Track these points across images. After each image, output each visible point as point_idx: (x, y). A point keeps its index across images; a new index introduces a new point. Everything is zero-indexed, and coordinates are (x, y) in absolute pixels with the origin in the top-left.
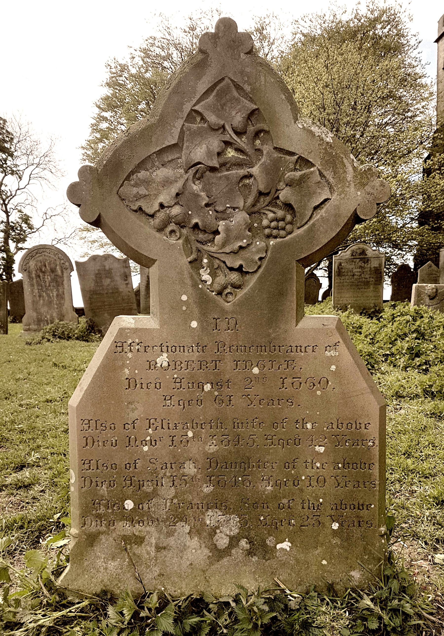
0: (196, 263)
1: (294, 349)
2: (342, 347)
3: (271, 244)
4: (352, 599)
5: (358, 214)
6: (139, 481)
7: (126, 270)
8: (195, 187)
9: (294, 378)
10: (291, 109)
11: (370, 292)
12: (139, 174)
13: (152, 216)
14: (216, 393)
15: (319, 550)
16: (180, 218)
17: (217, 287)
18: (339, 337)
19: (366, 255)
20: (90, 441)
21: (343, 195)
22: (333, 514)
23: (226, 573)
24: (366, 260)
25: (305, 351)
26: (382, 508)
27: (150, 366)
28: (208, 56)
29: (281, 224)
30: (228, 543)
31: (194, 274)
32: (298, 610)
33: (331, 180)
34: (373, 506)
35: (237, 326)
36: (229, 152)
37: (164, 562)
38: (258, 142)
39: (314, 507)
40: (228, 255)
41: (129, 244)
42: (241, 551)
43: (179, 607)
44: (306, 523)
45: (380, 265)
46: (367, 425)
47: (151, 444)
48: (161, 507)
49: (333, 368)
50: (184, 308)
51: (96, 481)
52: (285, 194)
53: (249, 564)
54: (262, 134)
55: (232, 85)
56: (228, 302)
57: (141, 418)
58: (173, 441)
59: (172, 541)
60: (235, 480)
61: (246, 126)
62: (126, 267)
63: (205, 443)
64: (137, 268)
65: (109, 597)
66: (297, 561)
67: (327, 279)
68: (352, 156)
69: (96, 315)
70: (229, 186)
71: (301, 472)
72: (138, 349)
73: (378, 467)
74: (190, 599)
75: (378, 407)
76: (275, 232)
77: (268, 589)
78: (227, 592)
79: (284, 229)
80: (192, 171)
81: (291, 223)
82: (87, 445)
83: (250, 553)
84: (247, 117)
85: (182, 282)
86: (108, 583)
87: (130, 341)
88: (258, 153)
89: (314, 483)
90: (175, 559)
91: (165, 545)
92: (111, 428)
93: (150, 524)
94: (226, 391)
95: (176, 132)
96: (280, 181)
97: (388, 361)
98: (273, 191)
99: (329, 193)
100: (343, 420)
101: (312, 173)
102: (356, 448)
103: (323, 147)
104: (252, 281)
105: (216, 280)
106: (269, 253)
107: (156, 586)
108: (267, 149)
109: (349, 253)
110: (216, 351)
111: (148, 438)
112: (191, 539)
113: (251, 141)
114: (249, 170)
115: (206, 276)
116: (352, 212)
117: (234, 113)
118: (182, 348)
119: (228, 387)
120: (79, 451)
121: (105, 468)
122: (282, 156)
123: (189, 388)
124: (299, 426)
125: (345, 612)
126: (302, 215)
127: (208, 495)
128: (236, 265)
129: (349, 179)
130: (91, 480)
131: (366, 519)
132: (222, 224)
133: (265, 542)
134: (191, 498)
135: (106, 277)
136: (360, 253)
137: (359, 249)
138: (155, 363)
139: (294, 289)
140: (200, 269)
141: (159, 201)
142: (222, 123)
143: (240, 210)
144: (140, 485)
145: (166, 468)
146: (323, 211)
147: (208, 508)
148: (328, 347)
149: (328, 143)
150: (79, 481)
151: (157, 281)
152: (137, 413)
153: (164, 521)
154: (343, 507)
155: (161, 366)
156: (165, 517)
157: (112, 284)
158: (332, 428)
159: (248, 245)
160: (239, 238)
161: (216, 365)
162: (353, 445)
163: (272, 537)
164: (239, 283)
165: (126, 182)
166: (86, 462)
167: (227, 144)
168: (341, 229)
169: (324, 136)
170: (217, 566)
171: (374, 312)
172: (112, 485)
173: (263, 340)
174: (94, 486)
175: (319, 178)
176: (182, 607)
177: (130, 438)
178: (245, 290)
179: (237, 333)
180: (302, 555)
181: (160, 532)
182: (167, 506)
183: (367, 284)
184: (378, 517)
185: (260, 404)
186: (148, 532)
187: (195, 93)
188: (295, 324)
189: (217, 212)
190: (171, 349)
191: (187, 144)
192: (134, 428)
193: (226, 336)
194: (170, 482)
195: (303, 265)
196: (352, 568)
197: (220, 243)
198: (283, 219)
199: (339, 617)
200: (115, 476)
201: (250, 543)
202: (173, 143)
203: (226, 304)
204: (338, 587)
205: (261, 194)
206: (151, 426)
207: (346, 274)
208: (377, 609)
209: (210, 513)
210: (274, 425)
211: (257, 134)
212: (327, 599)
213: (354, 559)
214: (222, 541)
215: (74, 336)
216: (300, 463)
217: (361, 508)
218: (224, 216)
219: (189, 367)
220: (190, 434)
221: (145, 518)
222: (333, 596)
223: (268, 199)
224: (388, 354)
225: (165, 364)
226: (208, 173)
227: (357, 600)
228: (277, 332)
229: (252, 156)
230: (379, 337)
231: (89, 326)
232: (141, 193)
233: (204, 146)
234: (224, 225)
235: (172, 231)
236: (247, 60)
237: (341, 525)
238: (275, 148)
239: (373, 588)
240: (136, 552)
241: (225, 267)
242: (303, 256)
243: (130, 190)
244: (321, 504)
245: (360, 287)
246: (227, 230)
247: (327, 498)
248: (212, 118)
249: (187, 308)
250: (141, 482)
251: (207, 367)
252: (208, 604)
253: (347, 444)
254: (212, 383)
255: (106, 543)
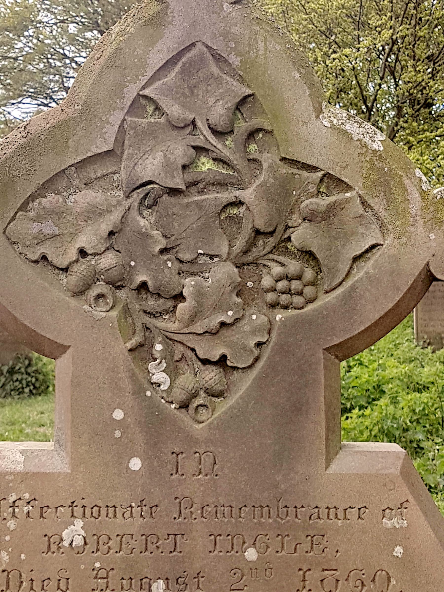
0: (141, 351)
1: (324, 512)
2: (413, 509)
3: (277, 319)
5: (433, 271)
8: (142, 222)
9: (324, 570)
10: (310, 95)
12: (44, 200)
13: (66, 270)
16: (115, 273)
17: (179, 395)
18: (408, 492)
21: (404, 240)
25: (345, 518)
27: (49, 546)
28: (167, 7)
29: (295, 285)
31: (137, 371)
33: (383, 213)
35: (216, 467)
36: (203, 164)
38: (253, 147)
40: (200, 338)
49: (399, 551)
50: (118, 434)
52: (301, 235)
54: (261, 135)
55: (208, 55)
61: (232, 123)
68: (418, 173)
70: (203, 220)
76: (284, 299)
79: (300, 293)
80: (137, 196)
81: (313, 283)
84: (234, 107)
87: (13, 497)
88: (252, 165)
95: (111, 132)
96: (292, 213)
98: (281, 228)
99: (379, 235)
101: (348, 200)
103: (368, 159)
104: (244, 384)
105: (177, 382)
106: (274, 334)
108: (268, 159)
110: (176, 515)
113: (242, 147)
114: (238, 193)
115: (159, 376)
116: (421, 268)
117: (211, 101)
118: (111, 510)
122: (296, 171)
126: (333, 271)
128: (215, 356)
129: (413, 212)
132: (189, 282)
138: (58, 541)
141: (78, 246)
142: (191, 117)
143: (222, 260)
146: (370, 264)
148: (388, 511)
149: (374, 151)
155: (71, 544)
159: (237, 320)
160: (218, 307)
164: (219, 387)
165: (20, 213)
167: (199, 150)
168: (403, 297)
169: (367, 139)
173: (266, 494)
175: (361, 210)
179: (215, 481)
187: (144, 68)
188: (324, 465)
189: (181, 262)
190: (92, 512)
191: (130, 151)
193: (194, 486)
195: (337, 357)
198: (299, 278)
202: (105, 149)
203: (196, 426)
205: (258, 232)
211: (251, 135)
218: (194, 269)
219: (124, 546)
223: (272, 241)
225: (78, 541)
226: (165, 197)
228: (291, 479)
229: (243, 172)
232: (46, 231)
233: (160, 154)
234: (192, 286)
235: (100, 296)
236: (234, 14)
238: (283, 159)
241: (194, 358)
242: (337, 341)
243: (26, 227)
246: (199, 294)
248: (174, 110)
249: (123, 433)
251: (158, 547)
254: (167, 579)
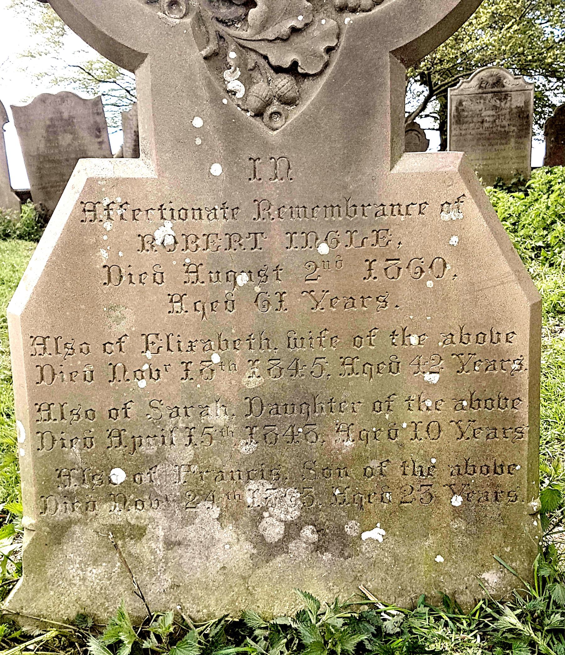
1: (388, 210)
2: (469, 204)
3: (346, 22)
4: (486, 617)
6: (133, 437)
7: (98, 119)
9: (387, 260)
11: (510, 149)
14: (258, 289)
15: (431, 540)
17: (254, 103)
18: (465, 187)
19: (504, 86)
20: (47, 372)
22: (453, 482)
23: (281, 580)
24: (503, 95)
25: (407, 214)
26: (533, 469)
27: (143, 245)
30: (282, 532)
32: (398, 635)
34: (518, 467)
35: (290, 171)
37: (180, 565)
39: (422, 472)
41: (98, 25)
42: (304, 545)
43: (206, 636)
44: (409, 498)
45: (527, 103)
46: (511, 335)
47: (151, 377)
48: (171, 477)
49: (454, 240)
50: (198, 141)
51: (62, 439)
53: (318, 565)
56: (274, 130)
57: (131, 333)
58: (187, 370)
59: (191, 532)
60: (293, 432)
62: (98, 114)
63: (241, 373)
64: (116, 119)
65: (90, 625)
66: (396, 558)
67: (438, 132)
69: (50, 199)
71: (401, 416)
72: (122, 215)
73: (527, 404)
74: (223, 622)
75: (529, 304)
77: (348, 602)
78: (283, 611)
82: (42, 379)
83: (319, 547)
85: (194, 95)
86: (89, 602)
89: (422, 433)
90: (197, 560)
91: (179, 538)
92: (81, 352)
93: (155, 505)
94: (274, 285)
97: (541, 258)
100: (471, 327)
102: (491, 375)
104: (314, 91)
106: (343, 39)
107: (168, 605)
109: (474, 83)
110: (255, 216)
111: (146, 367)
112: (223, 529)
115: (234, 84)
118: (197, 213)
119: (277, 279)
120: (29, 390)
121: (75, 417)
123: (211, 280)
124: (397, 340)
125: (475, 636)
127: (248, 458)
128: (286, 63)
130: (53, 437)
131: (507, 488)
133: (343, 529)
134: (220, 462)
135: (65, 131)
136: (494, 84)
137: (492, 76)
138: (151, 240)
139: (383, 129)
140: (224, 69)
144: (134, 442)
145: (178, 415)
147: (249, 478)
148: (446, 205)
150: (33, 438)
151: (148, 92)
152: (126, 323)
153: (178, 501)
154: (470, 470)
155: (162, 243)
156: (178, 494)
157: (76, 143)
158: (452, 342)
161: (256, 241)
162: (487, 369)
163: (354, 522)
164: (292, 94)
166: (42, 408)
170: (266, 569)
171: (518, 184)
172: (88, 444)
174: (58, 446)
176: (211, 635)
177: (114, 367)
178: (304, 107)
180: (403, 549)
181: (171, 518)
182: (182, 477)
183: (505, 136)
184: (526, 485)
185: (332, 306)
186: (152, 520)
188: (388, 166)
192: (121, 350)
193: (271, 190)
194: (184, 437)
196: (484, 567)
197: (258, 23)
199: (465, 644)
200: (93, 430)
201: (318, 531)
203: (271, 132)
204: (461, 599)
206: (150, 346)
207: (470, 119)
208: (527, 630)
209: (253, 485)
210: (356, 340)
212: (445, 617)
213: (488, 554)
214: (273, 531)
215: (15, 233)
216: (398, 403)
217: (499, 470)
219: (210, 244)
220: (216, 358)
221: (147, 497)
222: (454, 613)
224: (540, 247)
225: (169, 241)
227: (495, 619)
230: (524, 220)
231: (40, 216)
237: (467, 499)
239: (519, 598)
240: (132, 551)
241: (267, 66)
242: (402, 43)
244: (434, 467)
245: (493, 142)
247: (444, 457)
250: (137, 440)
251: (240, 245)
252: (252, 630)
253: (477, 368)
254: (250, 272)
255: (84, 537)
